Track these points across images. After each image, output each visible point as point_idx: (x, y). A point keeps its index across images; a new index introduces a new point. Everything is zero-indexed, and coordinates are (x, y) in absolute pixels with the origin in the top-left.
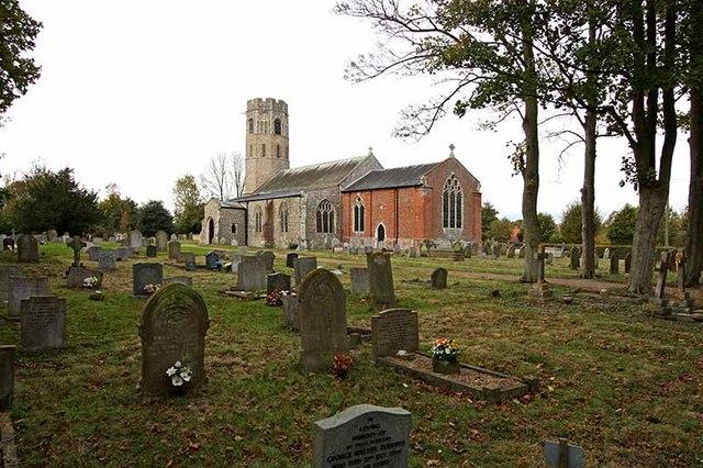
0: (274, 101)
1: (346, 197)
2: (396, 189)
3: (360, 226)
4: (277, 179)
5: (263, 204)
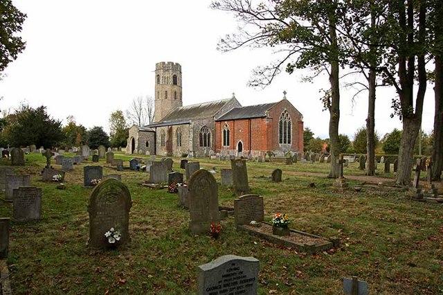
0: (173, 63)
1: (218, 124)
2: (249, 119)
3: (227, 142)
4: (175, 113)
5: (166, 129)
